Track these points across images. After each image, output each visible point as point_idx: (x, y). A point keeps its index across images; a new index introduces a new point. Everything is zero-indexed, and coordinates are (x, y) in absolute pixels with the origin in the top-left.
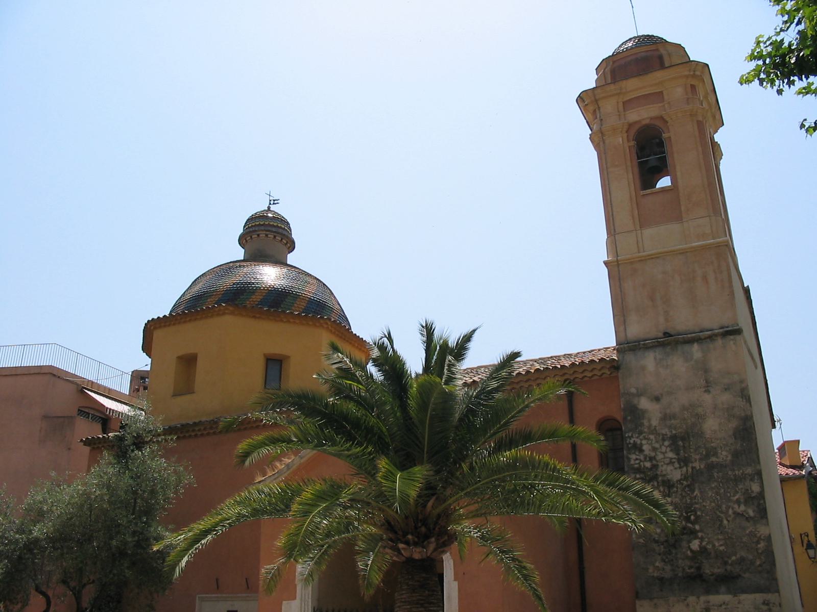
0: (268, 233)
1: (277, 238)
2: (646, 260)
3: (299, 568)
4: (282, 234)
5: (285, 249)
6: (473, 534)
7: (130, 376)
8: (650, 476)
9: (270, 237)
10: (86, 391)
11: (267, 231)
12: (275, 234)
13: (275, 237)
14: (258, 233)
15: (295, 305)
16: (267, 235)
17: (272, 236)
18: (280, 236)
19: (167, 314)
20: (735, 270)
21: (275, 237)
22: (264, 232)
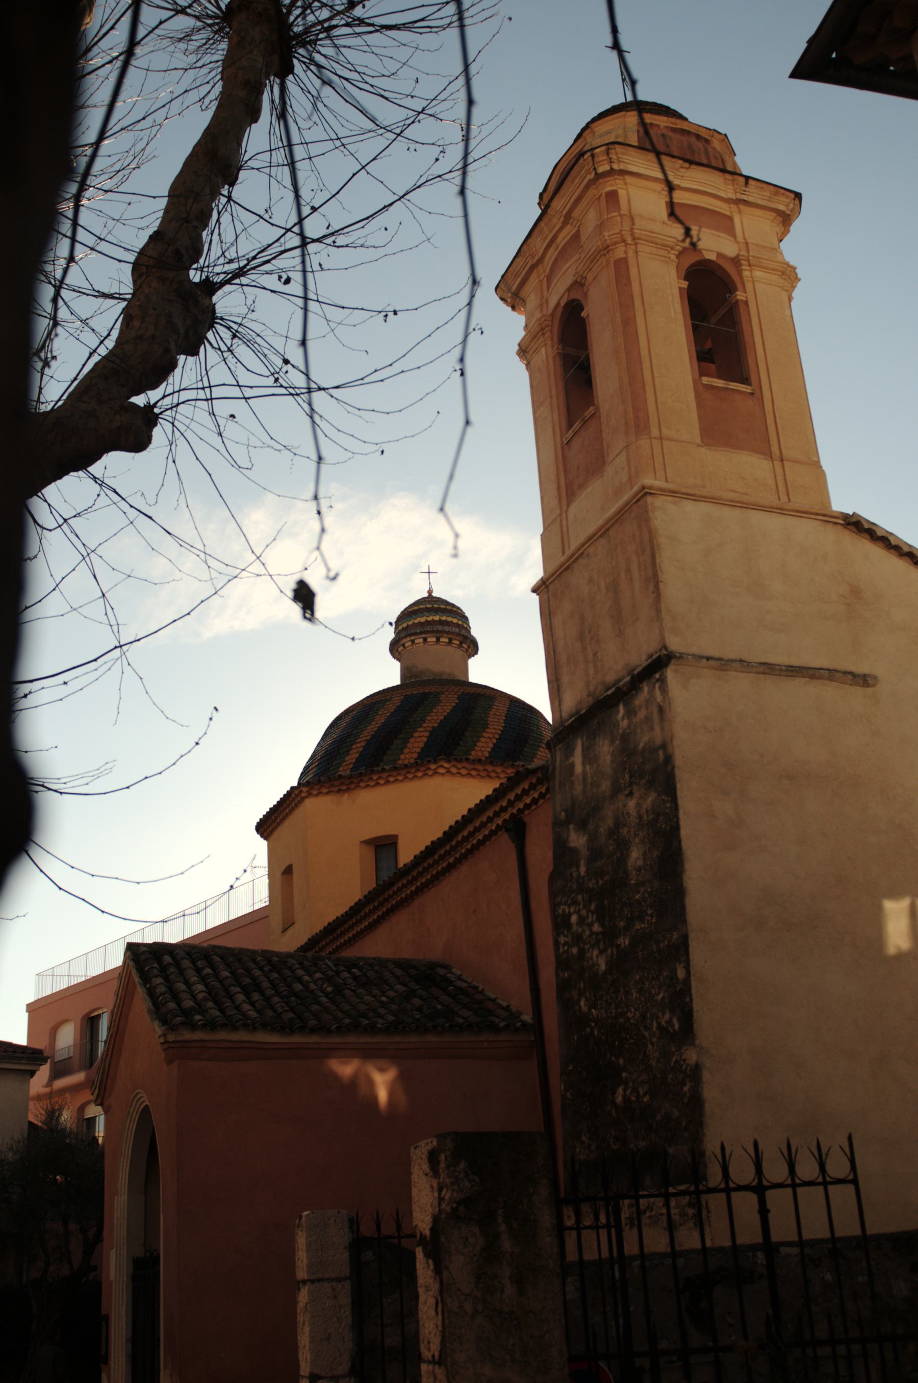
0: (413, 638)
1: (429, 640)
2: (777, 508)
3: (574, 994)
4: (459, 634)
5: (453, 652)
6: (648, 920)
7: (100, 1040)
8: (626, 253)
9: (418, 643)
10: (101, 1047)
11: (411, 635)
12: (424, 636)
13: (425, 640)
14: (402, 642)
15: (494, 707)
16: (413, 642)
17: (421, 640)
18: (445, 635)
19: (295, 784)
20: (813, 1151)
21: (425, 640)
22: (408, 639)
